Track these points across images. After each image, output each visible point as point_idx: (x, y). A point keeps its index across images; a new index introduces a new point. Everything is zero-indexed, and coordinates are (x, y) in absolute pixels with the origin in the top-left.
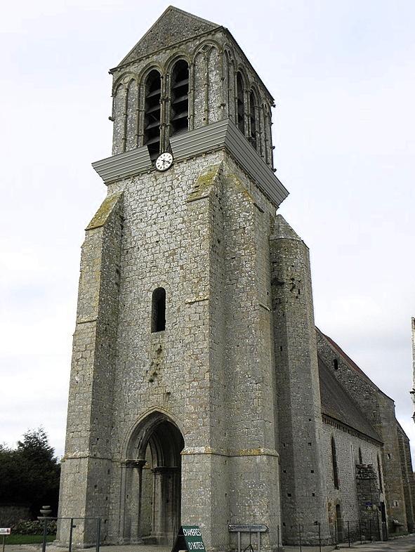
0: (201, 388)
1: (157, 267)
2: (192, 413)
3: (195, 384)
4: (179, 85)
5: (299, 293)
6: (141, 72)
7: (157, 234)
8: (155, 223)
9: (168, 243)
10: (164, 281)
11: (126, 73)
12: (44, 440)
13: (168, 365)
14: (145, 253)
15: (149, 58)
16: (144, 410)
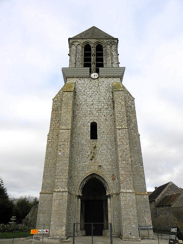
3: (124, 162)
7: (92, 101)
11: (76, 41)
12: (2, 184)
13: (100, 154)
14: (87, 107)
15: (87, 39)
16: (88, 172)
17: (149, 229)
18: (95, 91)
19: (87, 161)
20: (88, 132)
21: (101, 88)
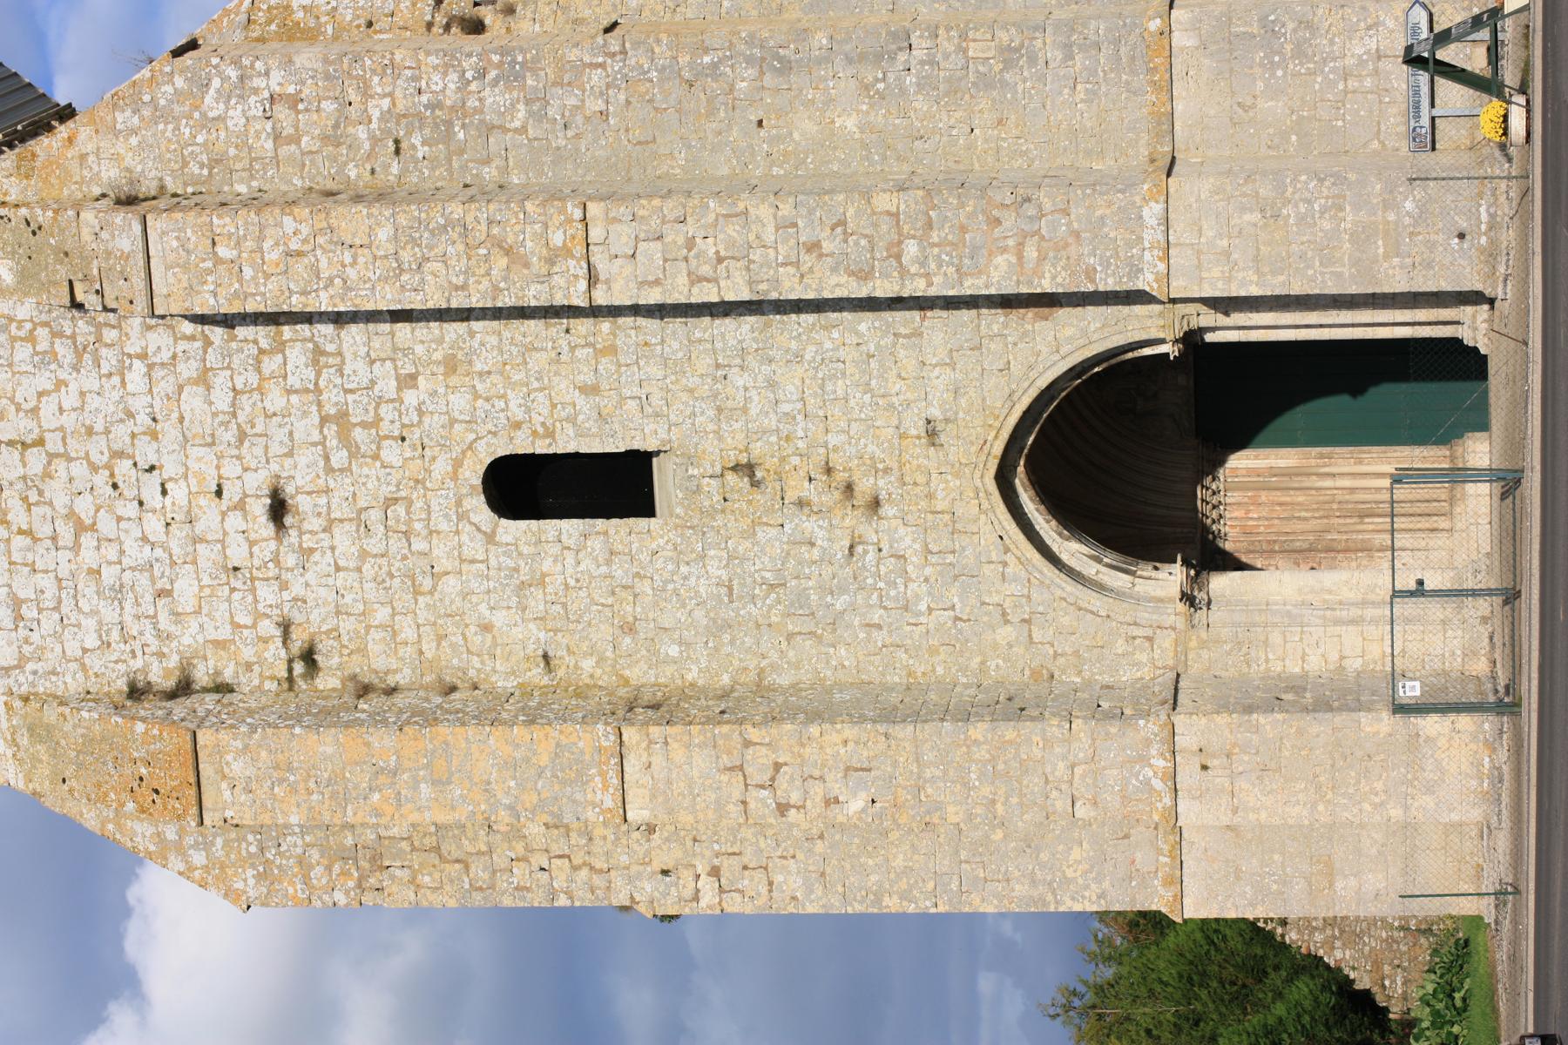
1: (391, 501)
2: (1020, 257)
3: (911, 248)
7: (240, 506)
9: (290, 454)
10: (458, 464)
14: (323, 562)
17: (1435, 112)
18: (101, 479)
19: (885, 547)
20: (596, 544)
21: (68, 420)
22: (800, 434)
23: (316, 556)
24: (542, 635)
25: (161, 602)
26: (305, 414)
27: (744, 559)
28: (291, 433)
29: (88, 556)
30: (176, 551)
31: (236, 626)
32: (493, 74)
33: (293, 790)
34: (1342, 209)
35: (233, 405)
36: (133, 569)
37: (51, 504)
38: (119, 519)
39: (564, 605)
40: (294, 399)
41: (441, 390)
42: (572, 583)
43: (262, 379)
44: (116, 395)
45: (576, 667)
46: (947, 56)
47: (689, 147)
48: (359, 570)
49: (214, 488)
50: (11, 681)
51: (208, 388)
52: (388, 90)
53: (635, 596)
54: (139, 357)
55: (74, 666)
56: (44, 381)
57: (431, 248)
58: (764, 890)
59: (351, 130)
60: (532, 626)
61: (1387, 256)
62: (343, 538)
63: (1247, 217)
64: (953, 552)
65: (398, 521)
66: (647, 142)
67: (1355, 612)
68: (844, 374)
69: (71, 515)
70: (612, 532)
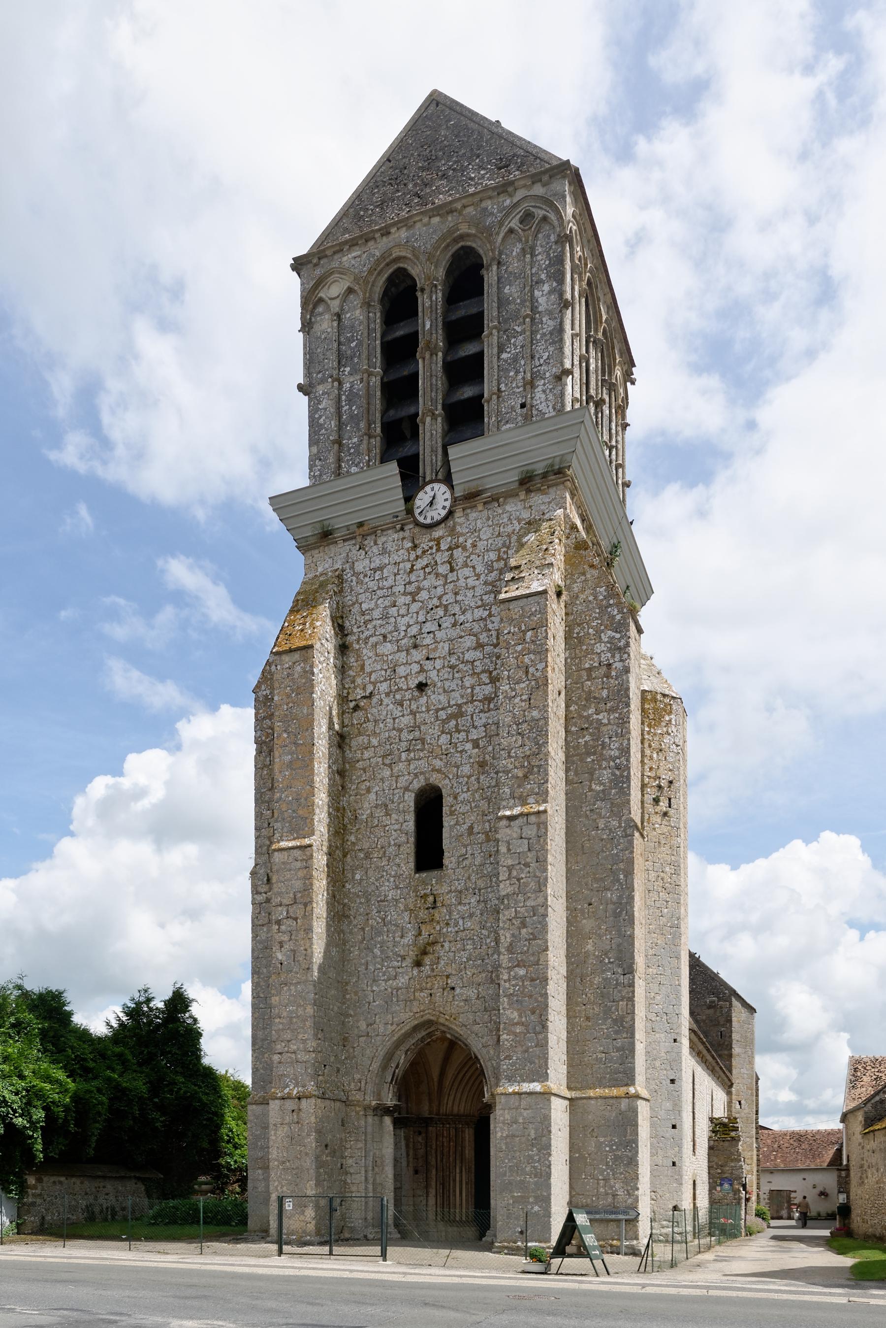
0: (533, 980)
1: (423, 741)
2: (517, 1024)
3: (522, 972)
4: (400, 333)
5: (670, 807)
6: (370, 272)
7: (422, 670)
8: (415, 646)
9: (445, 691)
10: (439, 771)
15: (389, 233)
16: (405, 1017)
19: (400, 970)
20: (403, 838)
21: (462, 582)
22: (449, 930)
23: (400, 709)
24: (365, 816)
25: (381, 638)
26: (462, 697)
27: (396, 906)
28: (454, 690)
29: (401, 600)
30: (403, 642)
31: (370, 674)
32: (618, 773)
33: (289, 696)
34: (536, 1176)
35: (467, 661)
36: (395, 622)
37: (425, 579)
38: (417, 613)
39: (377, 826)
40: (469, 690)
41: (471, 761)
42: (387, 828)
43: (478, 674)
44: (473, 604)
45: (351, 833)
46: (620, 992)
47: (580, 870)
48: (394, 729)
49: (431, 656)
50: (348, 570)
51: (475, 649)
52: (612, 721)
53: (381, 858)
54: (490, 613)
55: (354, 599)
56: (480, 568)
57: (528, 738)
58: (260, 923)
59: (593, 705)
60: (369, 811)
61: (513, 1197)
62: (407, 720)
63: (533, 1132)
64: (398, 1001)
65: (415, 745)
66: (583, 850)
67: (371, 1180)
68: (476, 948)
69: (419, 589)
70: (409, 845)
